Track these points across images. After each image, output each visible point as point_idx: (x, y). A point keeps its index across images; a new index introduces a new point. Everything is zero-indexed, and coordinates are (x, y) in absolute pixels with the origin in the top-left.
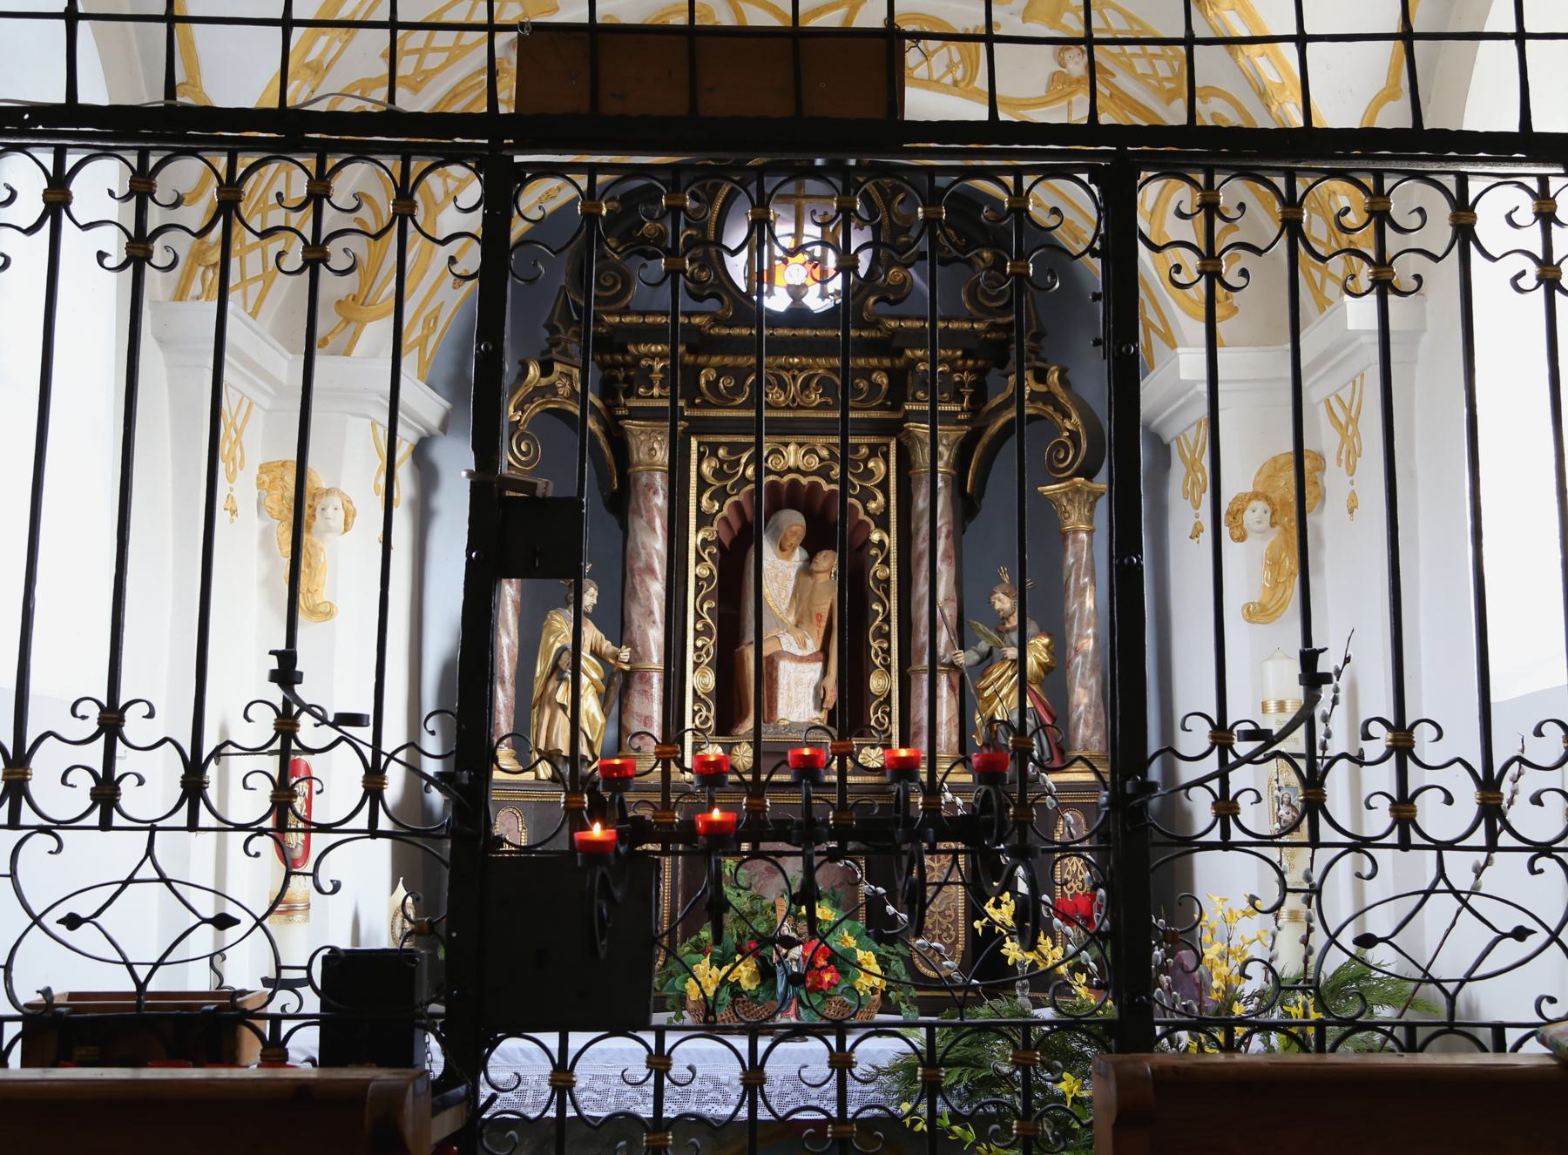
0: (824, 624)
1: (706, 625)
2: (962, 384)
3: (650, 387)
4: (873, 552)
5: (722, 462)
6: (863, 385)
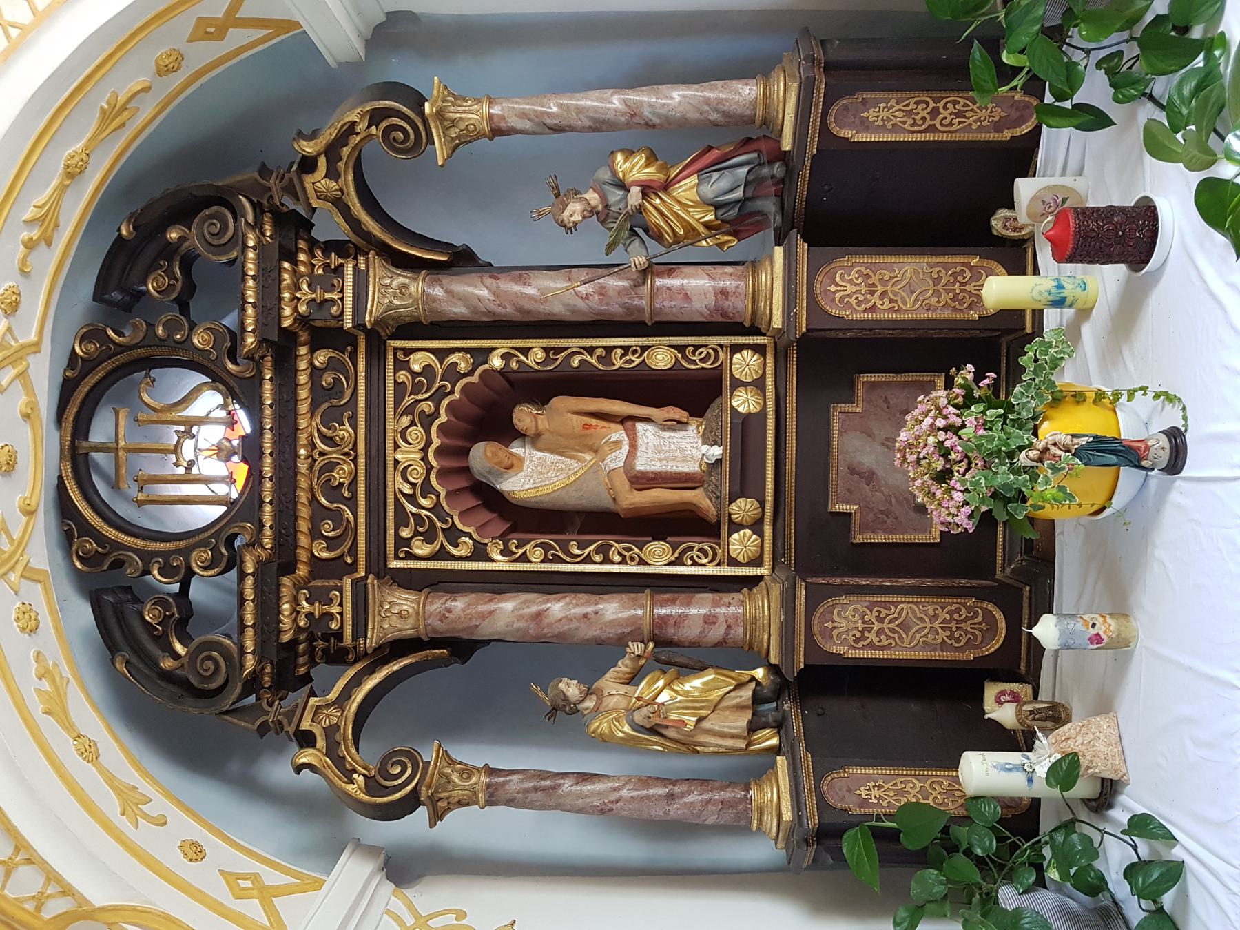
0: (594, 421)
1: (597, 551)
2: (326, 266)
3: (330, 616)
4: (514, 365)
5: (416, 533)
6: (327, 379)
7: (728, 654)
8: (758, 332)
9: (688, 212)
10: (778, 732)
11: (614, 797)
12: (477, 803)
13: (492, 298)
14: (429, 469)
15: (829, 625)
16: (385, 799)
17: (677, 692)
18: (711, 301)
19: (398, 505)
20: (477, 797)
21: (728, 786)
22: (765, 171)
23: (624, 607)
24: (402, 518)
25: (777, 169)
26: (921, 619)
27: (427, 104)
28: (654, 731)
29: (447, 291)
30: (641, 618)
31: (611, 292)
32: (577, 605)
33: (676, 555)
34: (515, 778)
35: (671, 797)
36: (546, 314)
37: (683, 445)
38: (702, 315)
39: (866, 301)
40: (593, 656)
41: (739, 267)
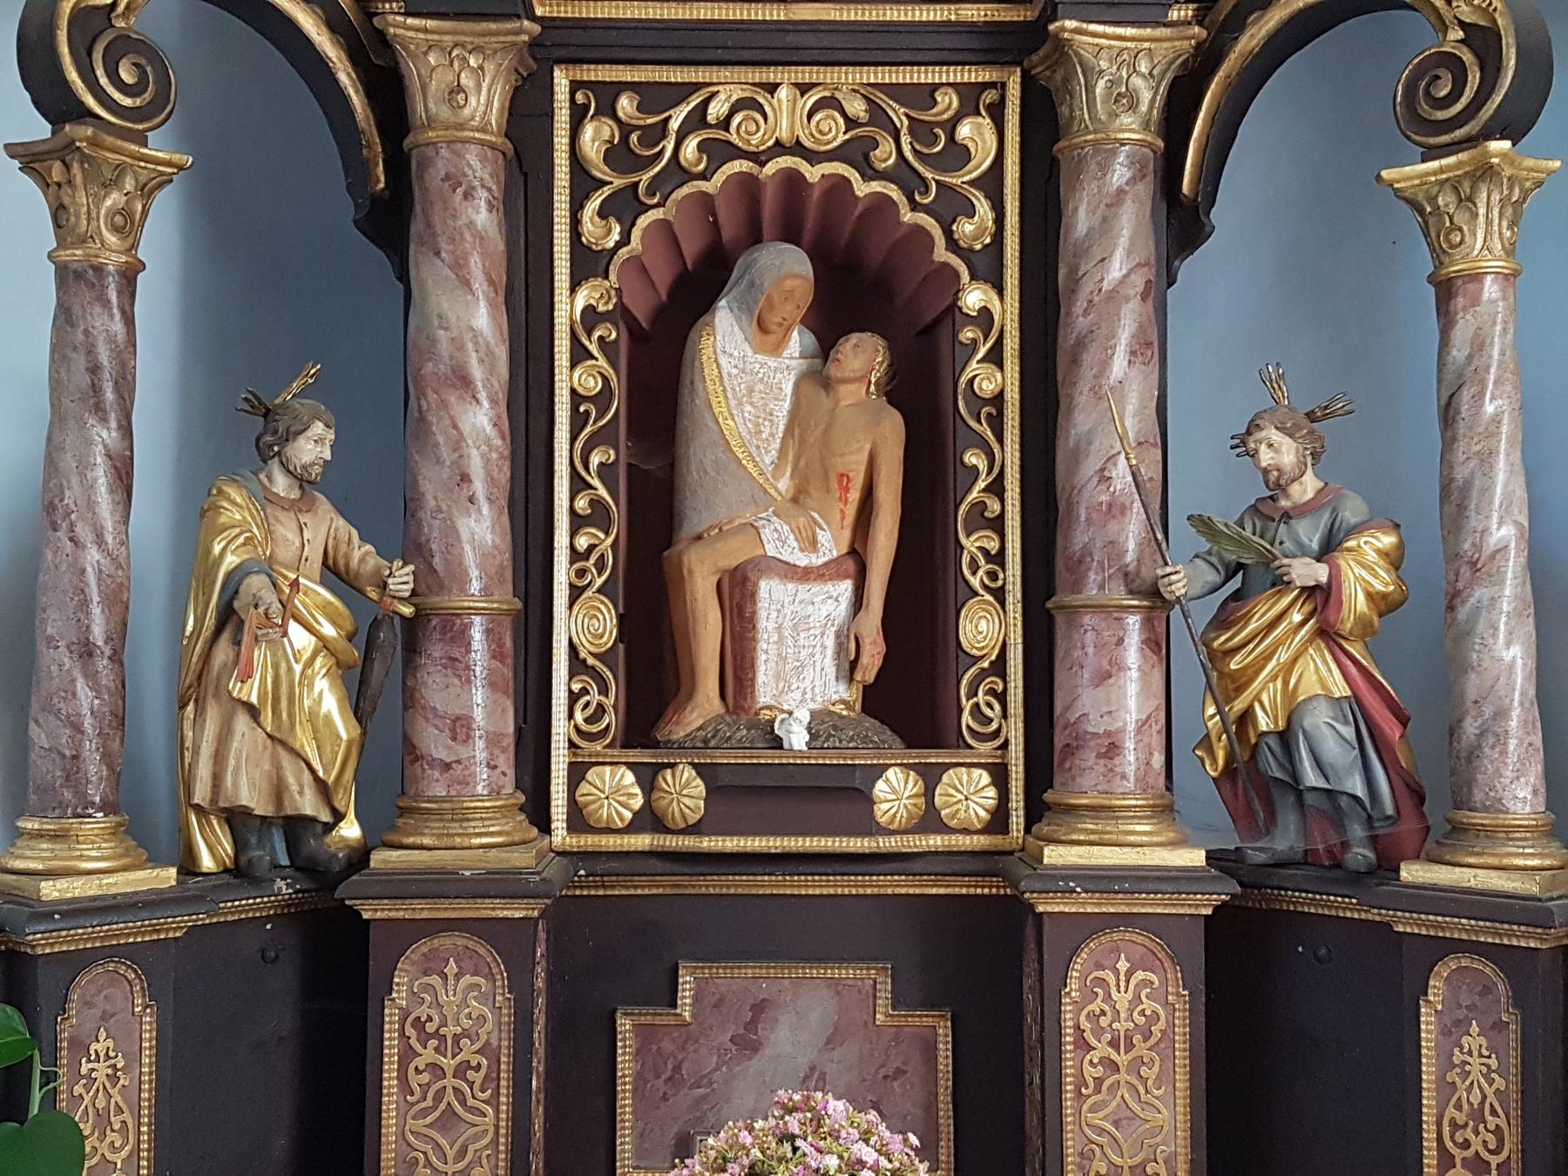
0: (855, 496)
1: (596, 503)
4: (968, 334)
5: (626, 129)
7: (391, 769)
8: (1031, 819)
9: (1274, 679)
10: (226, 871)
11: (84, 532)
12: (61, 244)
13: (1105, 286)
14: (759, 158)
15: (452, 968)
16: (64, 50)
17: (310, 662)
18: (1096, 725)
19: (685, 91)
20: (73, 246)
21: (111, 768)
22: (1357, 831)
23: (484, 557)
24: (657, 98)
25: (1361, 854)
26: (462, 1153)
27: (1507, 144)
28: (228, 616)
29: (1120, 191)
30: (463, 590)
31: (1113, 527)
32: (487, 460)
33: (591, 661)
34: (118, 327)
35: (86, 651)
36: (1071, 397)
37: (809, 674)
38: (1067, 708)
39: (1098, 1032)
40: (383, 490)
41: (1162, 780)
